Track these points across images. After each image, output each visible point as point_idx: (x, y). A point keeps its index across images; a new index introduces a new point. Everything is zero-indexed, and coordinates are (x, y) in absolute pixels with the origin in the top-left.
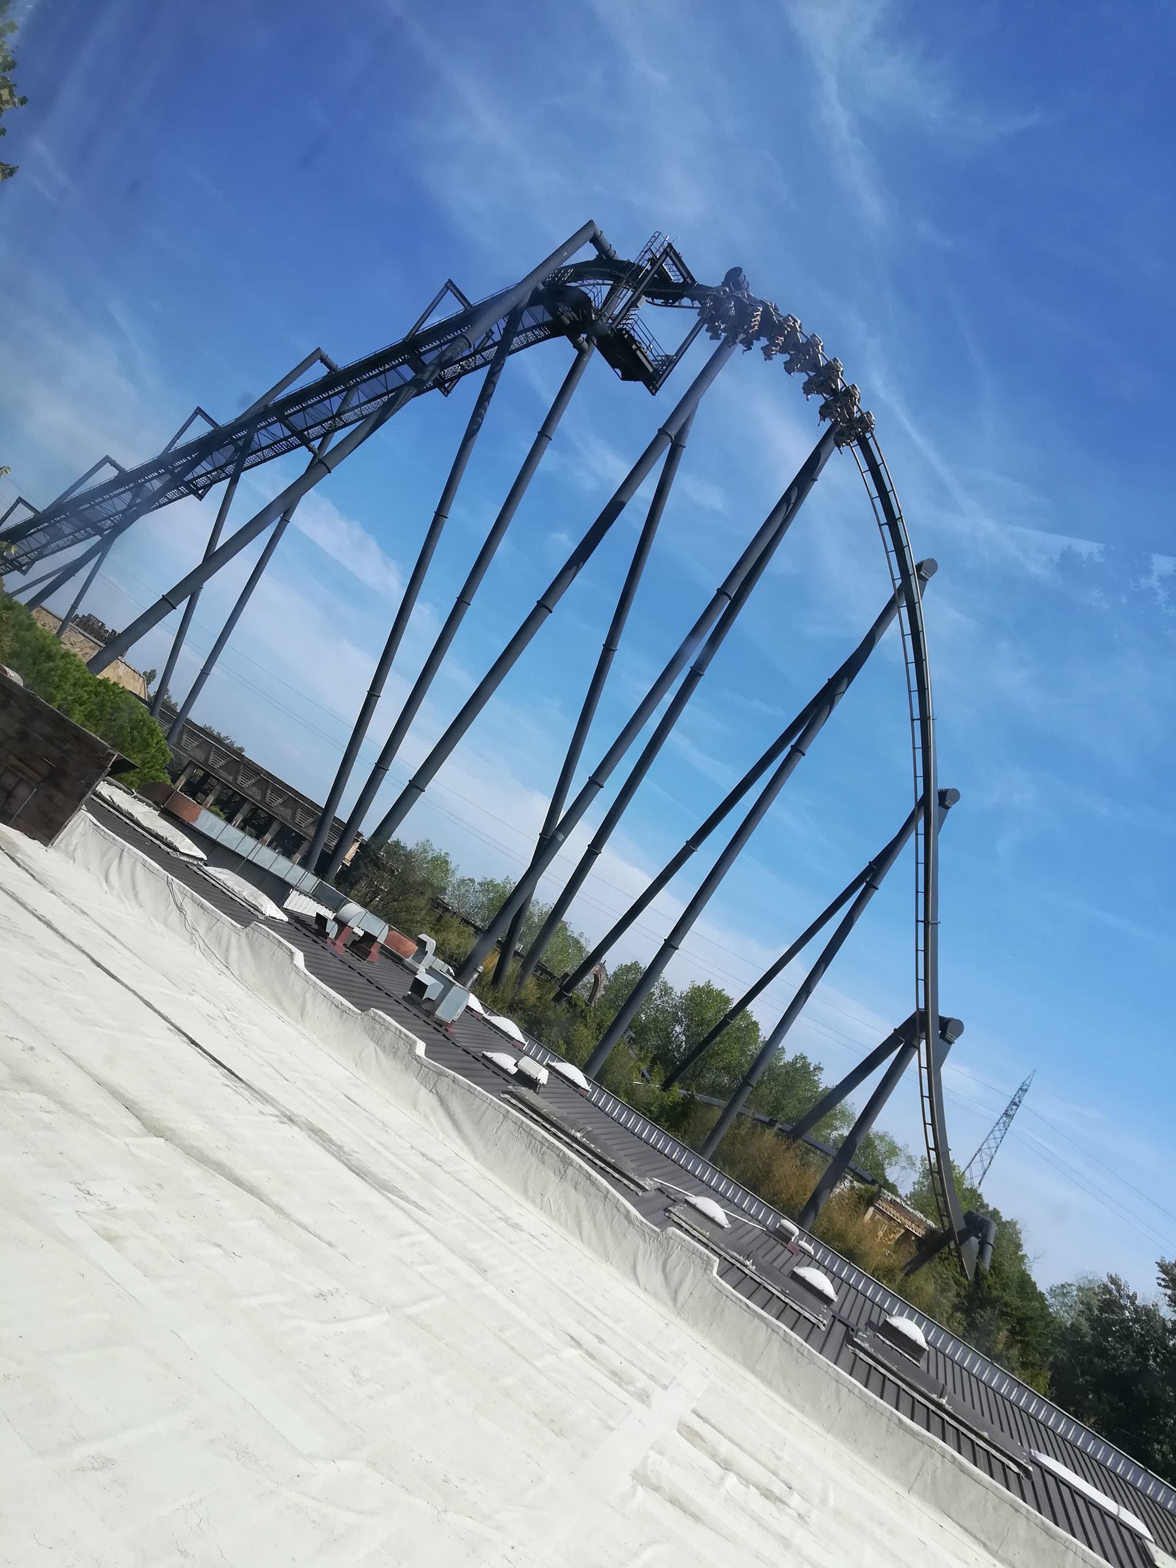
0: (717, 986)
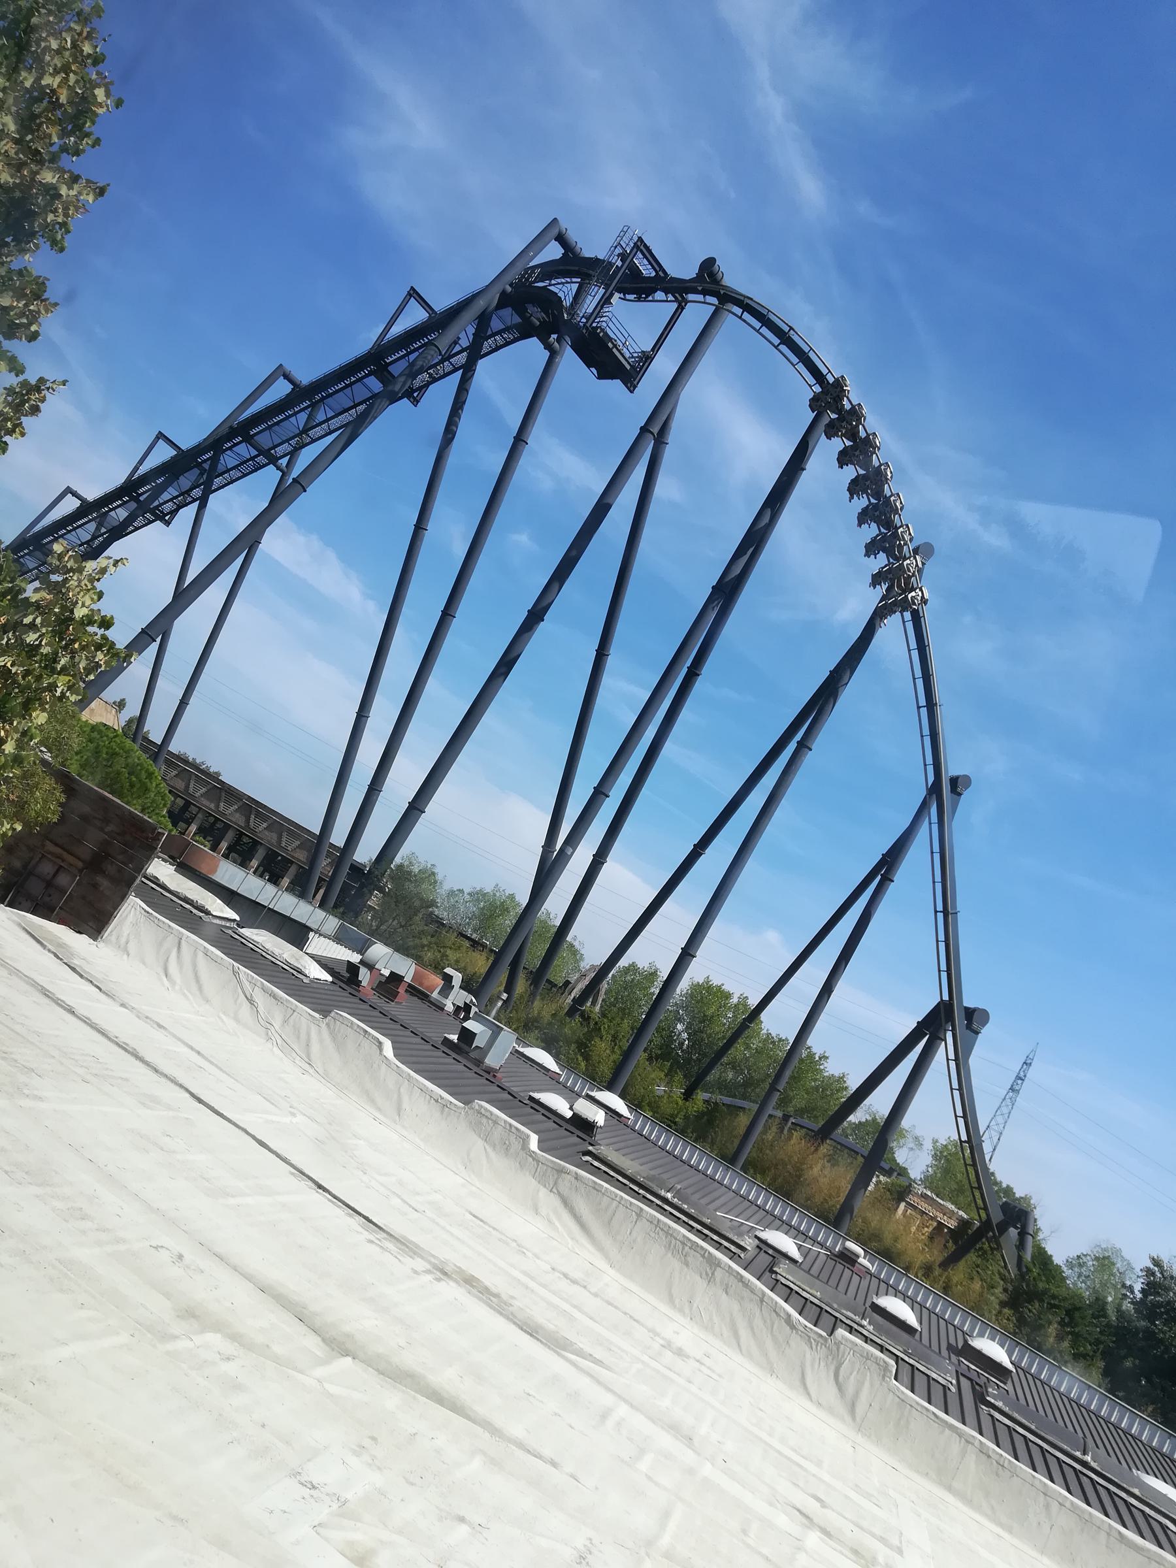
0: (715, 981)
